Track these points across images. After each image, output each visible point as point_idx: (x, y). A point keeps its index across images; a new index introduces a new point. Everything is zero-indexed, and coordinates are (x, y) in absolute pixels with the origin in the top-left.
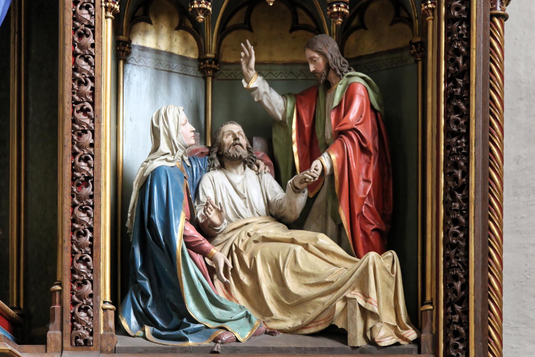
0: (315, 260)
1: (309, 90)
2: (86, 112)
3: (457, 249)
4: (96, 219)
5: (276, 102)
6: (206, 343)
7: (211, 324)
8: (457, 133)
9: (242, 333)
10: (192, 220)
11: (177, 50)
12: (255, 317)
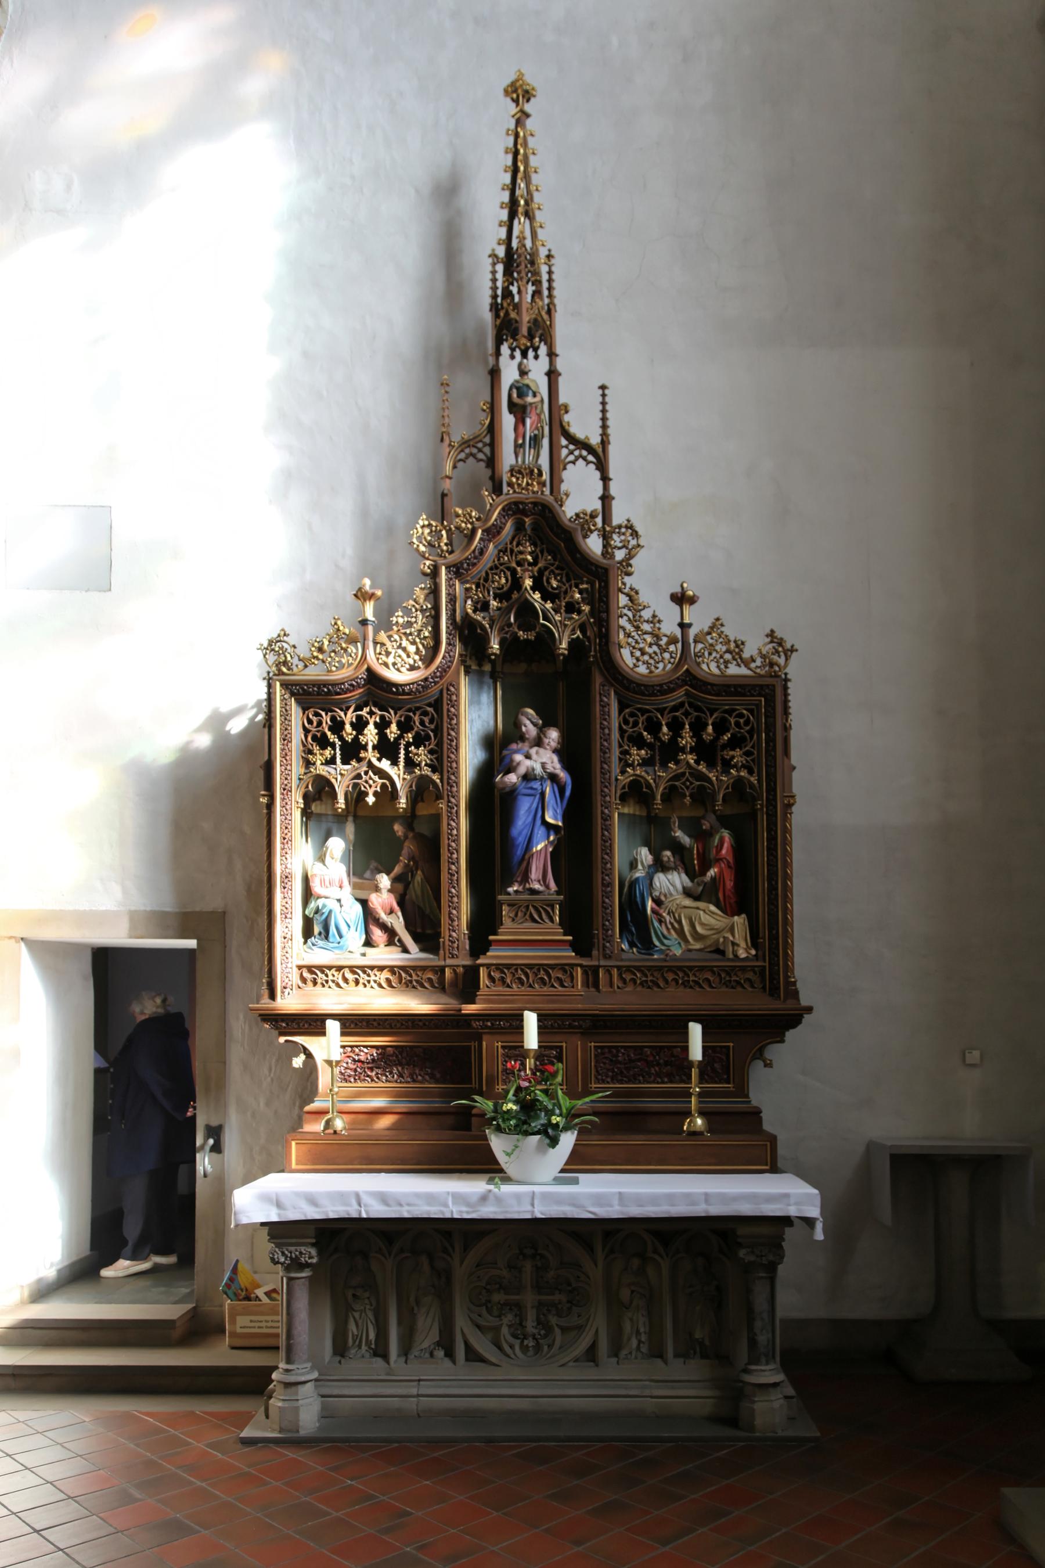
0: (709, 917)
1: (702, 836)
2: (607, 854)
3: (773, 916)
4: (613, 902)
5: (686, 840)
6: (662, 956)
7: (663, 948)
8: (772, 864)
9: (678, 952)
10: (654, 900)
11: (637, 813)
12: (682, 944)
